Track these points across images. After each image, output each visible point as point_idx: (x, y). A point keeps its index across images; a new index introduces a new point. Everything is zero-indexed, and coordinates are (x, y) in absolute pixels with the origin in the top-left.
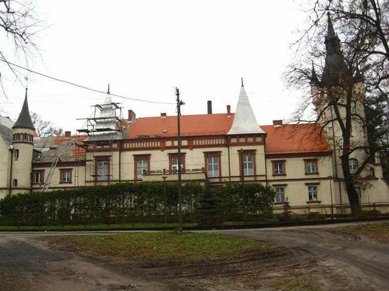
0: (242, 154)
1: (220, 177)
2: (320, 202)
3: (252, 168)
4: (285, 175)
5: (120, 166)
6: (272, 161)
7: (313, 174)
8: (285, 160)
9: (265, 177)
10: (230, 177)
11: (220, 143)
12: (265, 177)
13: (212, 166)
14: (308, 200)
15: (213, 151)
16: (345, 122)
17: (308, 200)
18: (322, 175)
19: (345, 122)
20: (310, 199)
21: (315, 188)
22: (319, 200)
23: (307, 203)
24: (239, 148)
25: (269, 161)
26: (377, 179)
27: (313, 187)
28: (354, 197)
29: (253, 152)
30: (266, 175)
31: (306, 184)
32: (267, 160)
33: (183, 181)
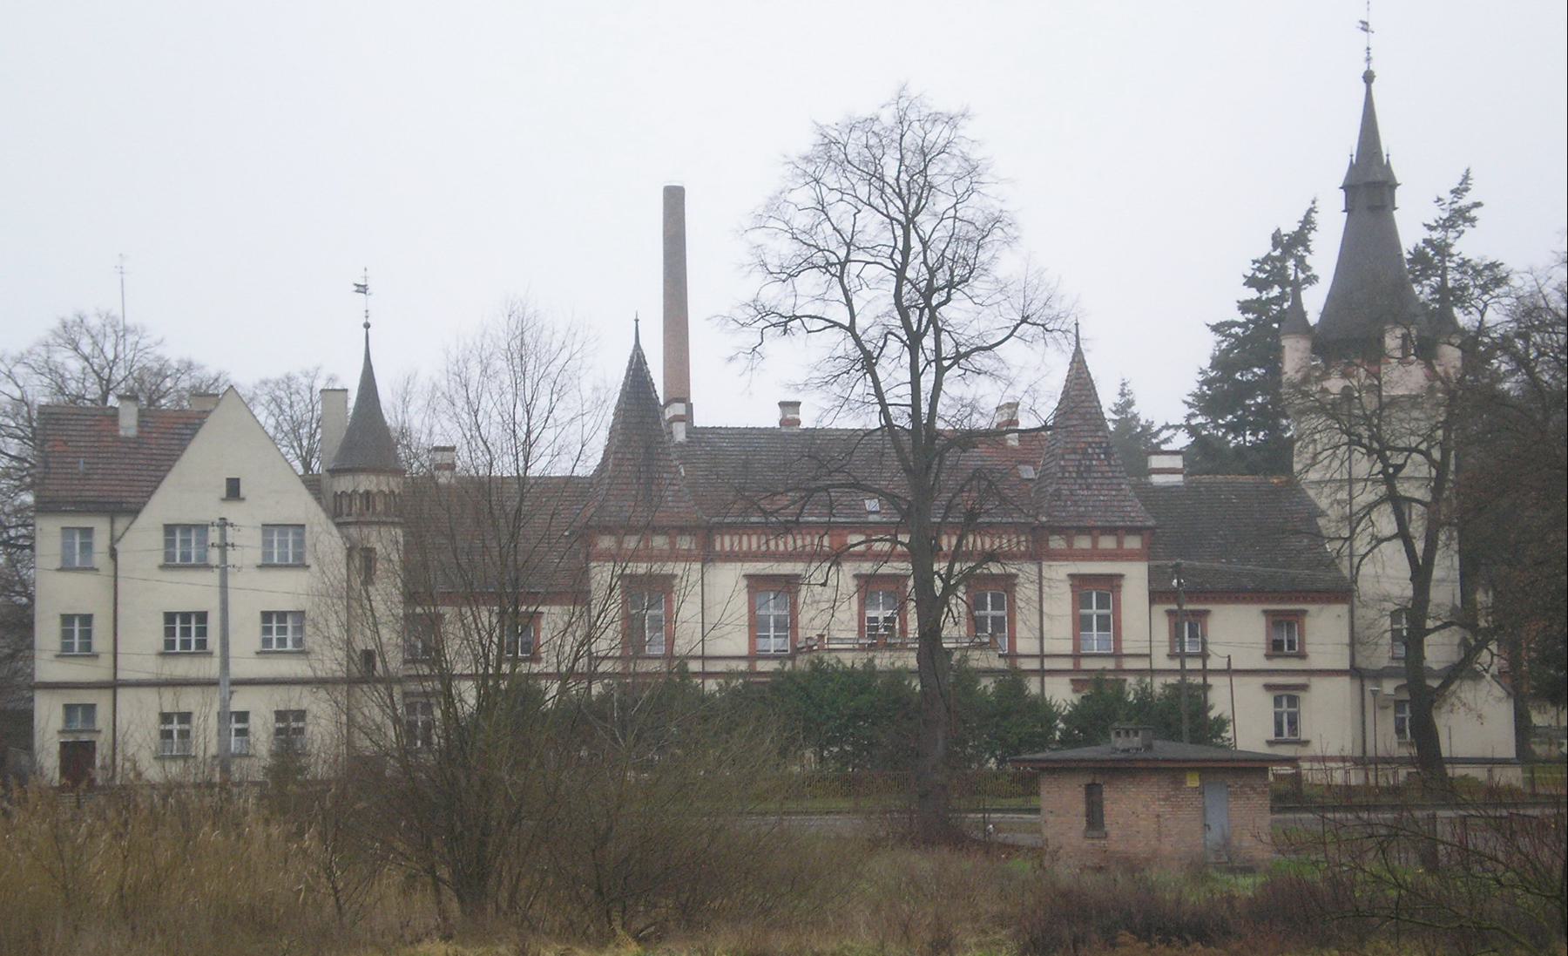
0: (1080, 584)
1: (1118, 655)
2: (1306, 743)
3: (1197, 636)
4: (1302, 656)
5: (116, 581)
6: (1265, 612)
7: (1287, 656)
8: (1207, 612)
9: (1148, 660)
10: (703, 658)
11: (763, 548)
12: (1148, 660)
13: (1091, 616)
14: (1272, 737)
15: (769, 571)
16: (1419, 546)
17: (1272, 737)
18: (1315, 662)
19: (1419, 546)
20: (1276, 735)
21: (1293, 701)
22: (1303, 737)
23: (1270, 743)
24: (867, 567)
25: (1159, 610)
26: (96, 656)
27: (1287, 697)
28: (1423, 733)
29: (1112, 583)
30: (1149, 656)
31: (1268, 687)
32: (759, 600)
33: (1210, 670)
